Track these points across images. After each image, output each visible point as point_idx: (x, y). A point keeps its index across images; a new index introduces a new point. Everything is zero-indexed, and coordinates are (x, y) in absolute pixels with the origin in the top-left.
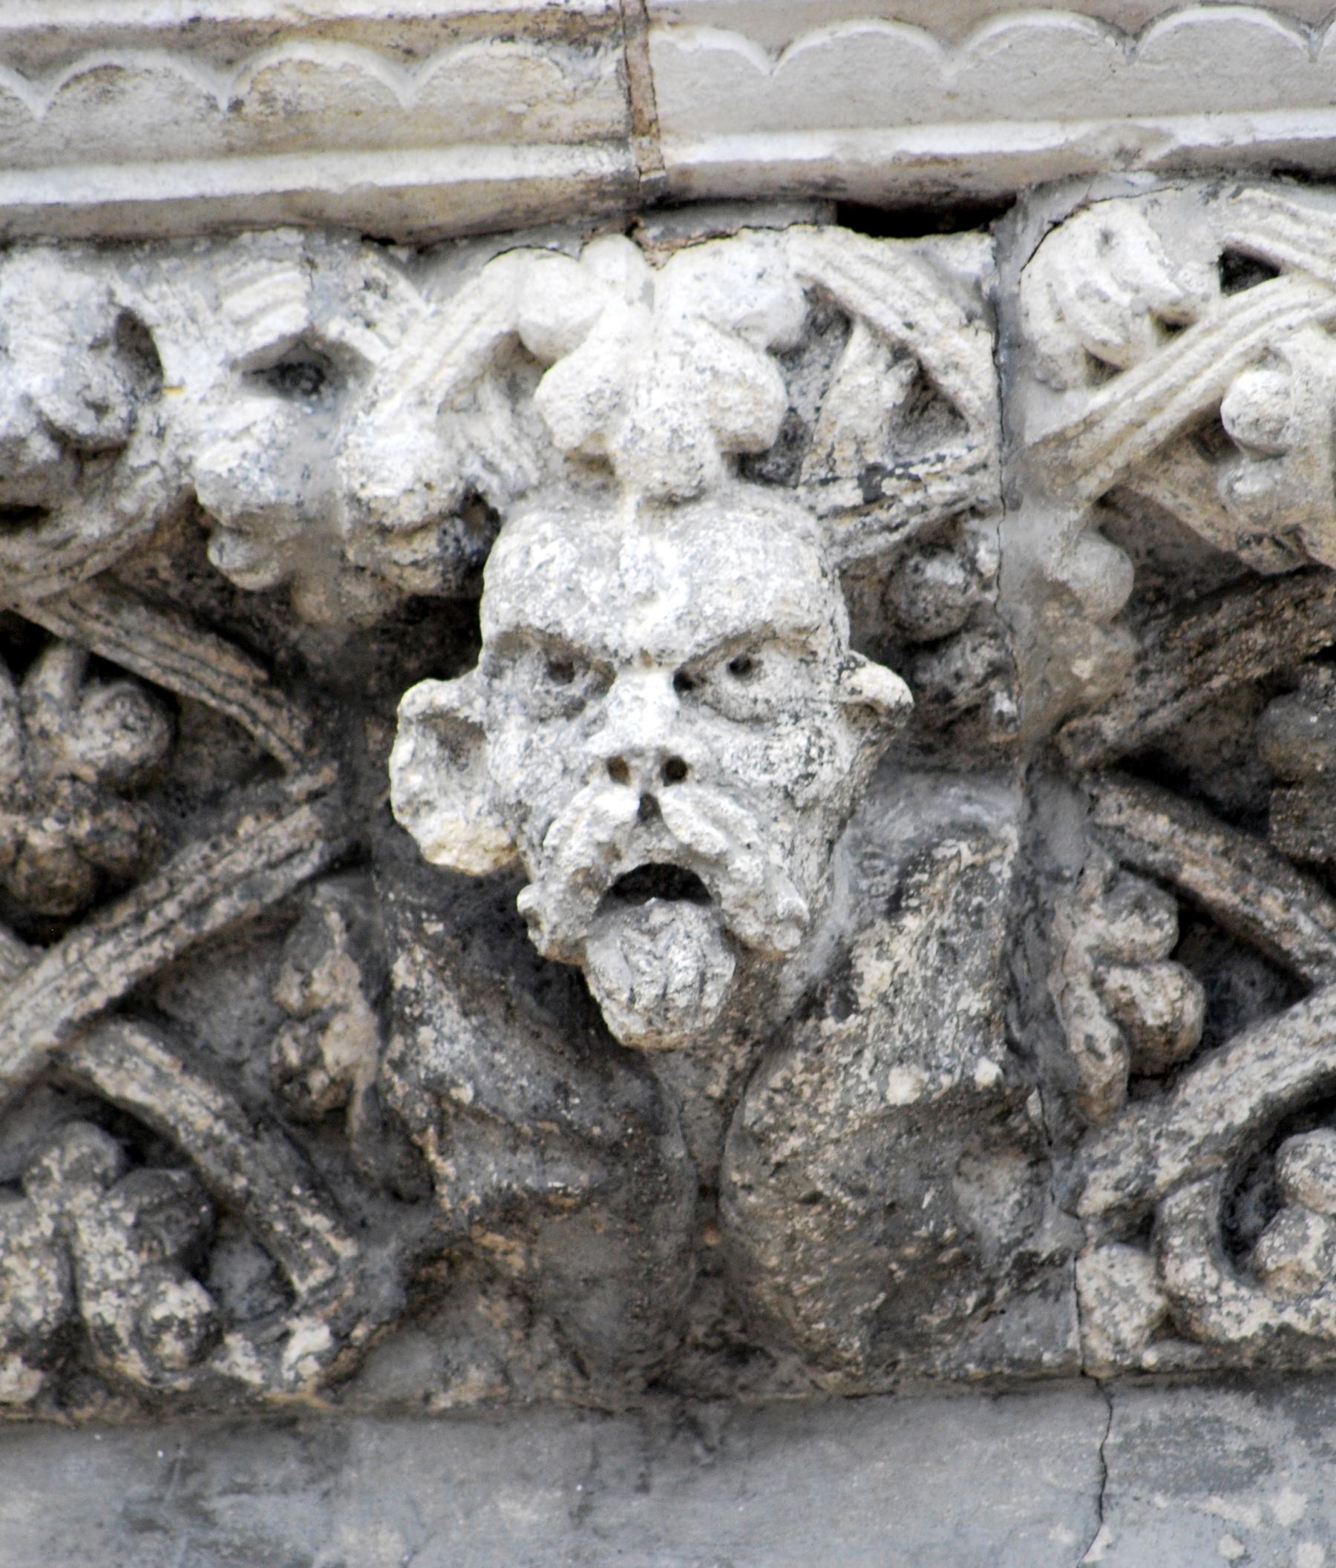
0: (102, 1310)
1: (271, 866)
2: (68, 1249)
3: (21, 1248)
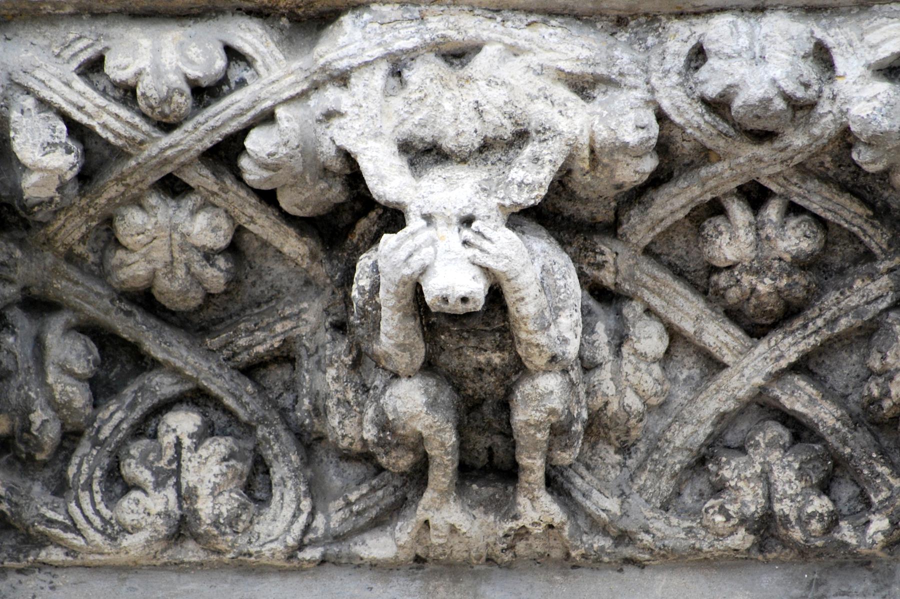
0: (783, 507)
1: (868, 303)
2: (767, 479)
3: (746, 477)
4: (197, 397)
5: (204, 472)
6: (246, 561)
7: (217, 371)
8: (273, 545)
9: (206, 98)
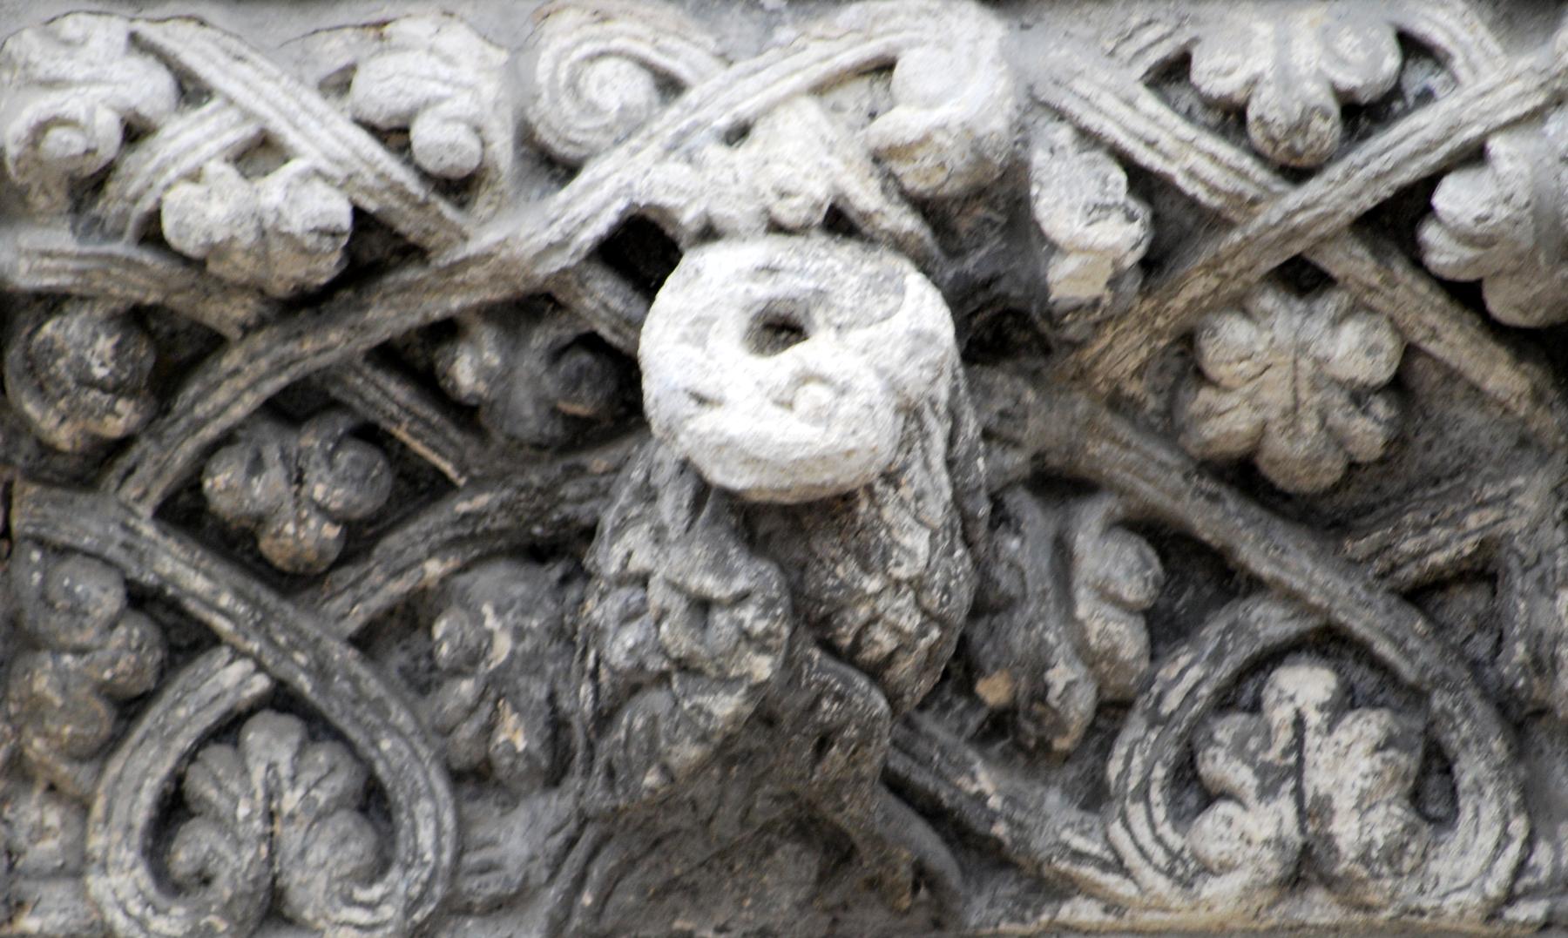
4: (1328, 642)
5: (1343, 769)
6: (1413, 924)
7: (1363, 596)
8: (1463, 896)
9: (1364, 123)
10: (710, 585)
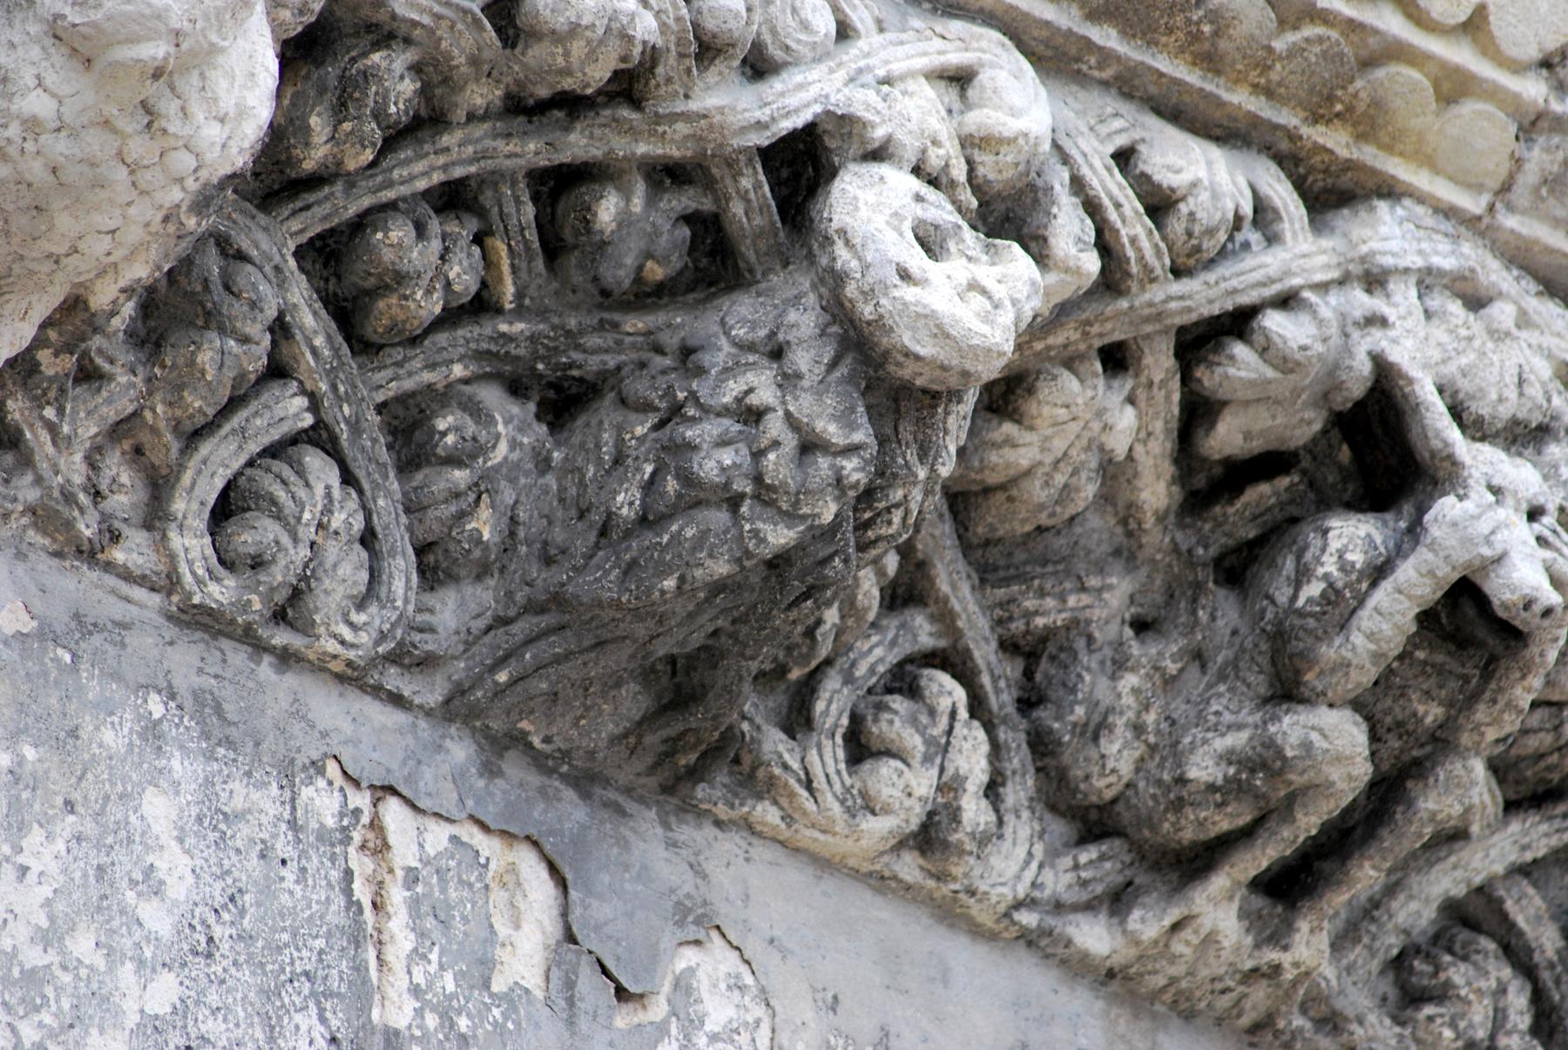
10: (832, 431)
